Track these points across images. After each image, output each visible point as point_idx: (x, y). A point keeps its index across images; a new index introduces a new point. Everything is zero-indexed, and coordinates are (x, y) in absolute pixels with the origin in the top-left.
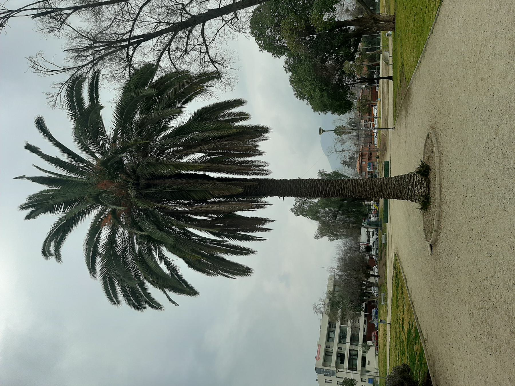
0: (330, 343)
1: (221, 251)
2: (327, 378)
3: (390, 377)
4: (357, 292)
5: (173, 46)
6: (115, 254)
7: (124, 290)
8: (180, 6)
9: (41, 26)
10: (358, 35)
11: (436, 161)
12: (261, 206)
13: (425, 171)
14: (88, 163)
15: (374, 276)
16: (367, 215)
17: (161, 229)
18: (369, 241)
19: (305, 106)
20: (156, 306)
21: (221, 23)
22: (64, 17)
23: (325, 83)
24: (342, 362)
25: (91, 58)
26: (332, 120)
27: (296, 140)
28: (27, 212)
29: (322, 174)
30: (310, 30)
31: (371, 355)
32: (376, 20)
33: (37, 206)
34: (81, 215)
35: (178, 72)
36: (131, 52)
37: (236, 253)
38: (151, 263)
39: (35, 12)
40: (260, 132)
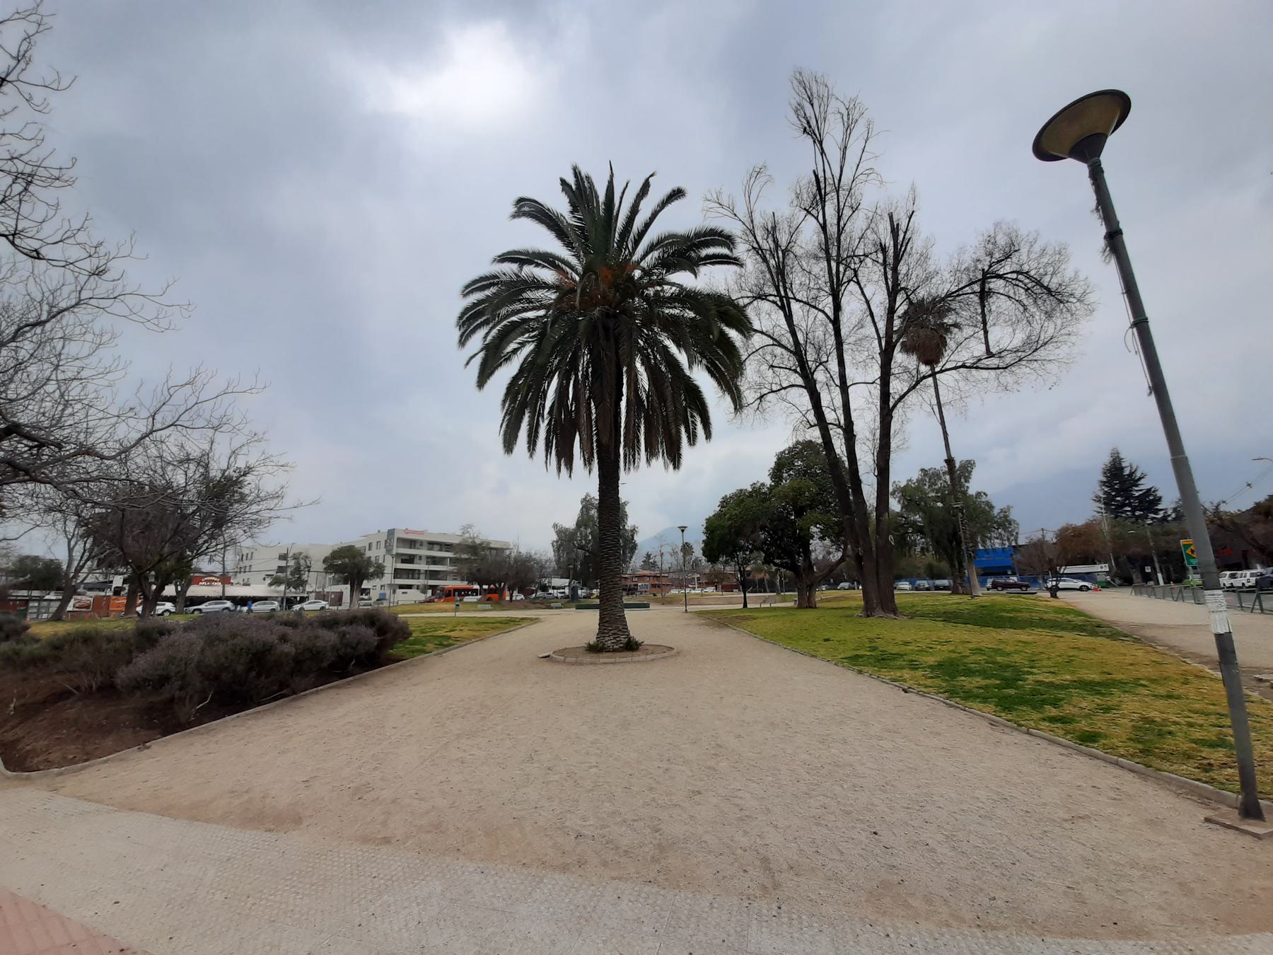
0: (426, 546)
1: (532, 418)
2: (383, 544)
3: (396, 618)
4: (494, 576)
5: (778, 350)
6: (524, 291)
7: (480, 302)
8: (824, 359)
9: (804, 182)
10: (793, 567)
11: (642, 657)
12: (588, 462)
13: (632, 646)
14: (631, 254)
15: (511, 596)
16: (585, 585)
17: (554, 347)
18: (554, 588)
19: (712, 508)
20: (463, 341)
21: (804, 409)
22: (814, 212)
23: (739, 532)
24: (403, 561)
25: (765, 246)
26: (697, 538)
27: (669, 499)
28: (571, 180)
29: (634, 531)
30: (799, 512)
31: (415, 596)
32: (811, 587)
33: (579, 191)
34: (569, 245)
35: (742, 363)
36: (771, 298)
37: (529, 436)
38: (512, 335)
39: (821, 174)
40: (675, 457)
